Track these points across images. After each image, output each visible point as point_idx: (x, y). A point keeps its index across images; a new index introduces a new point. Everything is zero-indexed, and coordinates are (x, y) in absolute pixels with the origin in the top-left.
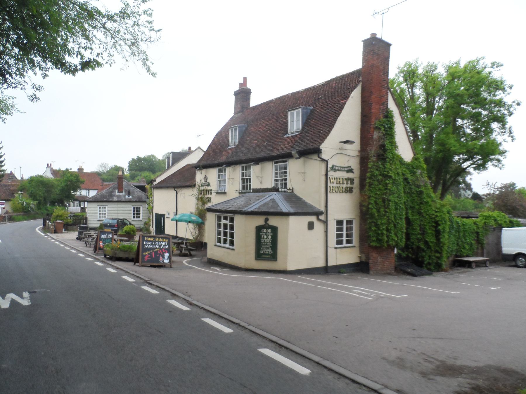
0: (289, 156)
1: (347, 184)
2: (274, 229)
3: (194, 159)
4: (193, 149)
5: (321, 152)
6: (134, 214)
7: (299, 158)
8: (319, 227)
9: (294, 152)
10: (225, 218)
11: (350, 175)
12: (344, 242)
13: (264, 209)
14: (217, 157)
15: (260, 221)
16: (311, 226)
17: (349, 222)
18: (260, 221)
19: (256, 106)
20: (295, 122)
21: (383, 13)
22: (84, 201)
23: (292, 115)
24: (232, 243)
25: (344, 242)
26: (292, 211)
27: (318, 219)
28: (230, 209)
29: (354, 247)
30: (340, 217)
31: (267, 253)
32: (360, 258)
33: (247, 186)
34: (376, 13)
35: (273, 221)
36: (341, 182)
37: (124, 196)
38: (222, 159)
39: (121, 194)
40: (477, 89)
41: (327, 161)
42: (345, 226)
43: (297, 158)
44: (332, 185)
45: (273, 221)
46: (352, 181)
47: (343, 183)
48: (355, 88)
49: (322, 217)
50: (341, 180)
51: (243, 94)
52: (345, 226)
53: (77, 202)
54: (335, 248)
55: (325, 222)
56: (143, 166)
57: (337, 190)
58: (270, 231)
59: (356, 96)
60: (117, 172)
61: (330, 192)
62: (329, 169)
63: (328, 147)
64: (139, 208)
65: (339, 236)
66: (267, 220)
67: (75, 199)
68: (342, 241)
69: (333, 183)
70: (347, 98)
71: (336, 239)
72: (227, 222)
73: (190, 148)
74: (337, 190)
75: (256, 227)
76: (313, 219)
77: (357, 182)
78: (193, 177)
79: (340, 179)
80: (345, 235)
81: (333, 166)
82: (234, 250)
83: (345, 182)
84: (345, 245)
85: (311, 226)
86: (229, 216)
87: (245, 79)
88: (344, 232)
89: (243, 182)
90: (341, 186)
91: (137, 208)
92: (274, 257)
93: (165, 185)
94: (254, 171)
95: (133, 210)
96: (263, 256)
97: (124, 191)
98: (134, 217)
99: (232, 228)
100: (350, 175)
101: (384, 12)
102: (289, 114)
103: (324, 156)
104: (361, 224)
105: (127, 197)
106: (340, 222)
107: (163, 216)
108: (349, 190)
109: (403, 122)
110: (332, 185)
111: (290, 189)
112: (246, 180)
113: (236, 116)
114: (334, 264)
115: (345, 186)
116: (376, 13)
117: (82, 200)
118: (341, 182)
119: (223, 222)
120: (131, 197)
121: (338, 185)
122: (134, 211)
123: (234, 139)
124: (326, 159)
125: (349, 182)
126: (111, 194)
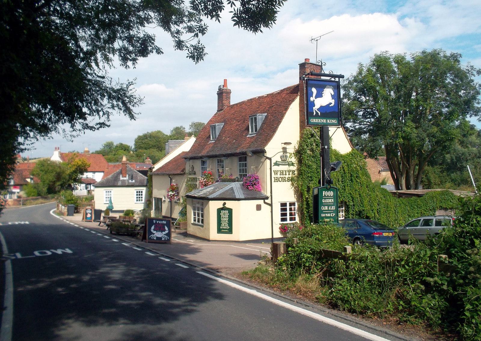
1: (289, 175)
2: (230, 211)
8: (266, 208)
12: (288, 219)
13: (224, 197)
16: (259, 208)
17: (292, 204)
21: (317, 40)
22: (90, 184)
24: (202, 222)
25: (288, 219)
26: (243, 197)
27: (265, 203)
30: (284, 201)
31: (225, 228)
33: (243, 167)
34: (313, 39)
35: (229, 204)
37: (128, 181)
38: (204, 153)
39: (125, 179)
40: (430, 82)
41: (270, 159)
47: (286, 175)
48: (293, 100)
49: (268, 201)
51: (223, 94)
55: (271, 205)
62: (273, 164)
64: (142, 192)
66: (225, 204)
67: (80, 181)
70: (286, 109)
76: (261, 202)
81: (276, 161)
83: (287, 173)
85: (259, 208)
87: (225, 81)
88: (288, 212)
89: (246, 164)
91: (139, 192)
92: (230, 231)
95: (136, 193)
96: (223, 230)
97: (127, 176)
101: (318, 39)
103: (268, 155)
105: (130, 181)
106: (283, 205)
115: (287, 176)
116: (313, 39)
117: (89, 183)
118: (284, 174)
120: (134, 181)
121: (282, 176)
122: (137, 195)
125: (291, 173)
126: (116, 178)
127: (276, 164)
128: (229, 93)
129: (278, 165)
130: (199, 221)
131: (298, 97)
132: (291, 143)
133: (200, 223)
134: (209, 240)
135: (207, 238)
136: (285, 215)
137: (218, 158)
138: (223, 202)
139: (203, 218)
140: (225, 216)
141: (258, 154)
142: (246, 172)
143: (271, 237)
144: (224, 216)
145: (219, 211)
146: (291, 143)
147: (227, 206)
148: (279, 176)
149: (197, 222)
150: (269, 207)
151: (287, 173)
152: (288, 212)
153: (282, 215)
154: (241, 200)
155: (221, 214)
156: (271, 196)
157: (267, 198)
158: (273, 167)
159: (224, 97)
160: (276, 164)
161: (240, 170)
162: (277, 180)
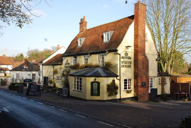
0: (105, 52)
3: (62, 51)
4: (60, 46)
11: (130, 60)
14: (73, 51)
18: (92, 79)
19: (89, 29)
24: (81, 89)
27: (117, 79)
35: (98, 79)
41: (120, 55)
46: (131, 63)
48: (131, 23)
49: (118, 78)
50: (126, 62)
52: (128, 87)
53: (3, 71)
55: (120, 80)
56: (35, 54)
58: (97, 84)
59: (132, 27)
62: (121, 58)
63: (121, 49)
66: (95, 79)
70: (128, 28)
72: (79, 80)
73: (58, 46)
77: (133, 63)
78: (62, 61)
80: (128, 86)
82: (81, 92)
86: (79, 78)
92: (98, 95)
93: (47, 64)
99: (81, 82)
100: (130, 60)
103: (119, 52)
106: (125, 80)
107: (48, 78)
108: (130, 67)
109: (145, 47)
110: (122, 64)
115: (127, 65)
121: (125, 64)
125: (129, 63)
127: (123, 58)
128: (86, 23)
129: (124, 58)
130: (78, 89)
131: (134, 22)
133: (79, 90)
134: (86, 100)
135: (84, 98)
146: (131, 46)
147: (97, 80)
148: (123, 64)
149: (76, 90)
150: (119, 81)
152: (128, 84)
154: (164, 89)
156: (120, 75)
157: (118, 76)
160: (123, 58)
162: (123, 66)
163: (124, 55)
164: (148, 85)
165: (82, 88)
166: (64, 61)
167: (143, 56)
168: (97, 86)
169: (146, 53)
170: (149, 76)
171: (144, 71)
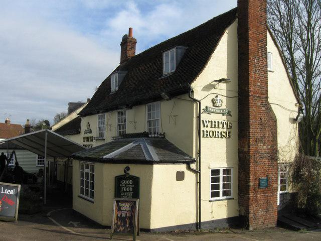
1: (223, 128)
2: (136, 181)
5: (193, 92)
6: (38, 161)
7: (170, 99)
8: (190, 177)
9: (163, 94)
10: (87, 168)
12: (221, 194)
15: (119, 170)
16: (180, 176)
17: (226, 171)
18: (119, 170)
20: (169, 65)
23: (167, 56)
24: (92, 196)
25: (221, 194)
26: (158, 160)
27: (189, 168)
28: (91, 156)
29: (233, 199)
30: (215, 166)
32: (240, 211)
35: (135, 170)
36: (217, 126)
42: (221, 176)
43: (167, 100)
44: (205, 129)
45: (135, 170)
47: (218, 127)
49: (193, 166)
50: (217, 124)
52: (221, 176)
54: (210, 201)
55: (197, 172)
57: (211, 135)
60: (243, 149)
61: (203, 137)
62: (202, 111)
65: (215, 187)
66: (128, 169)
68: (219, 192)
69: (207, 126)
71: (211, 191)
74: (211, 135)
75: (116, 177)
76: (182, 167)
79: (215, 122)
80: (221, 186)
82: (93, 202)
83: (221, 126)
84: (221, 197)
85: (180, 176)
86: (90, 163)
87: (130, 29)
90: (217, 130)
94: (130, 114)
98: (38, 164)
102: (164, 54)
104: (240, 173)
106: (215, 172)
110: (205, 129)
111: (161, 135)
112: (121, 126)
113: (122, 65)
114: (210, 219)
118: (217, 126)
119: (86, 170)
121: (213, 130)
123: (114, 87)
124: (198, 99)
127: (207, 110)
128: (134, 42)
129: (210, 113)
132: (202, 90)
136: (217, 187)
137: (119, 110)
138: (124, 166)
139: (94, 172)
140: (128, 189)
141: (178, 97)
142: (99, 122)
143: (192, 220)
144: (125, 189)
145: (118, 180)
150: (194, 175)
151: (221, 126)
152: (221, 183)
153: (213, 187)
155: (121, 185)
157: (193, 161)
158: (202, 115)
159: (128, 47)
161: (119, 119)
163: (210, 105)
164: (275, 185)
165: (95, 191)
166: (83, 127)
167: (264, 109)
168: (131, 189)
169: (270, 101)
170: (269, 69)
171: (265, 147)
